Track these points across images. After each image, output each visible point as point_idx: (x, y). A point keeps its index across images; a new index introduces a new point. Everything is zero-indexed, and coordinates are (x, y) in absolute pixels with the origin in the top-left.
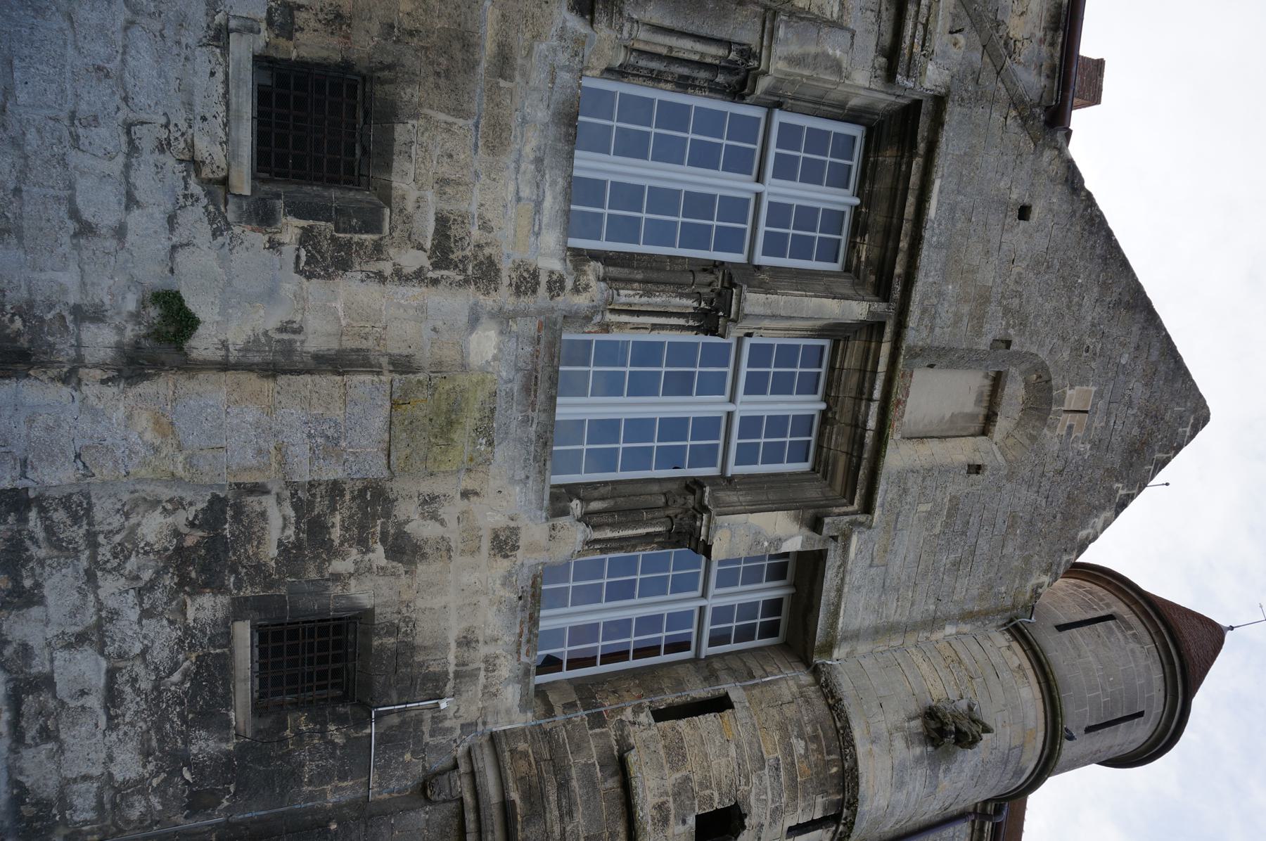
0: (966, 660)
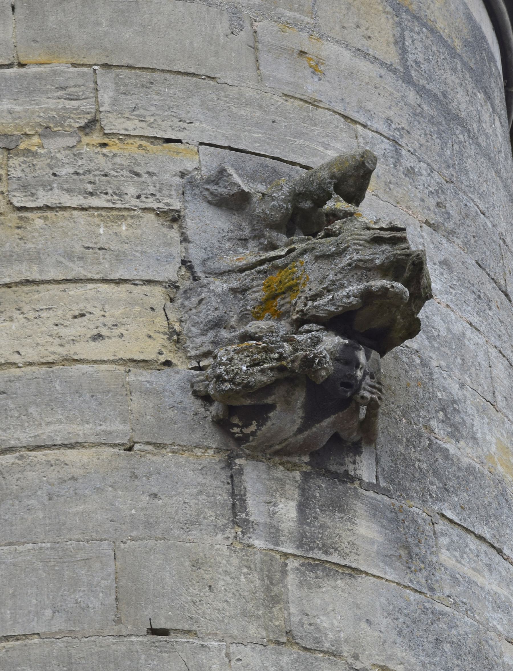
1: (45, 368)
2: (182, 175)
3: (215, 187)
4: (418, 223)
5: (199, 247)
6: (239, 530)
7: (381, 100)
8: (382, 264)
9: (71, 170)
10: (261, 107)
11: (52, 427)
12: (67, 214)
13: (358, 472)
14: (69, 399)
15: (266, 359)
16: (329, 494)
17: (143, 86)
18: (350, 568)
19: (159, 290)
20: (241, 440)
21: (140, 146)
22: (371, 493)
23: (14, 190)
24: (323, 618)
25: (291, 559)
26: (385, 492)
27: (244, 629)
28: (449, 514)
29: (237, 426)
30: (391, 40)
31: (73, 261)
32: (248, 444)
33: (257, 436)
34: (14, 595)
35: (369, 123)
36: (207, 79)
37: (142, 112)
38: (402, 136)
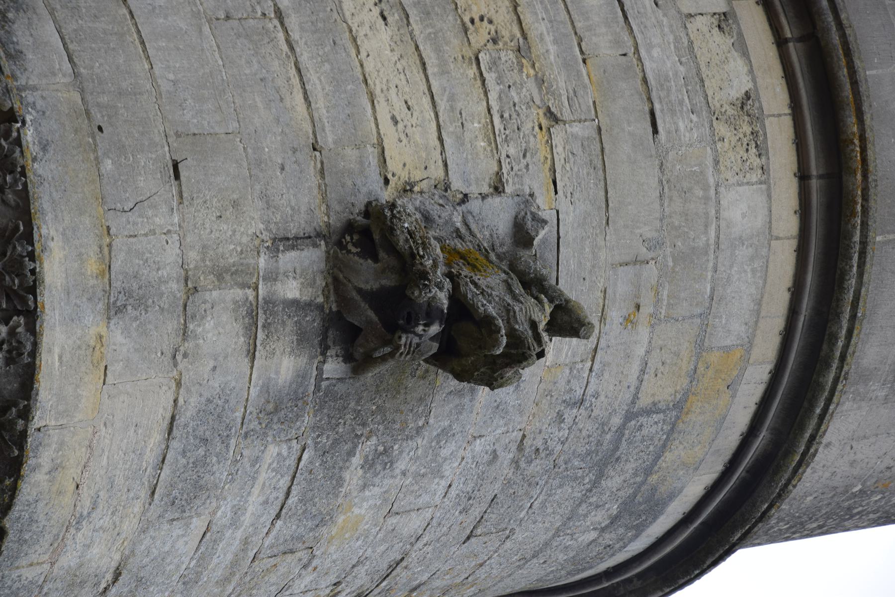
0: (548, 47)
1: (361, 77)
2: (532, 195)
4: (523, 426)
5: (481, 209)
6: (269, 244)
7: (611, 388)
8: (516, 330)
9: (516, 100)
10: (593, 267)
11: (317, 82)
12: (482, 96)
13: (330, 359)
14: (342, 96)
15: (418, 244)
17: (591, 161)
18: (255, 351)
19: (441, 173)
20: (340, 244)
21: (547, 158)
22: (315, 373)
23: (490, 54)
24: (212, 324)
25: (254, 293)
26: (317, 387)
27: (192, 247)
28: (305, 456)
29: (352, 239)
30: (656, 399)
31: (448, 101)
34: (178, 49)
37: (572, 160)
38: (586, 409)
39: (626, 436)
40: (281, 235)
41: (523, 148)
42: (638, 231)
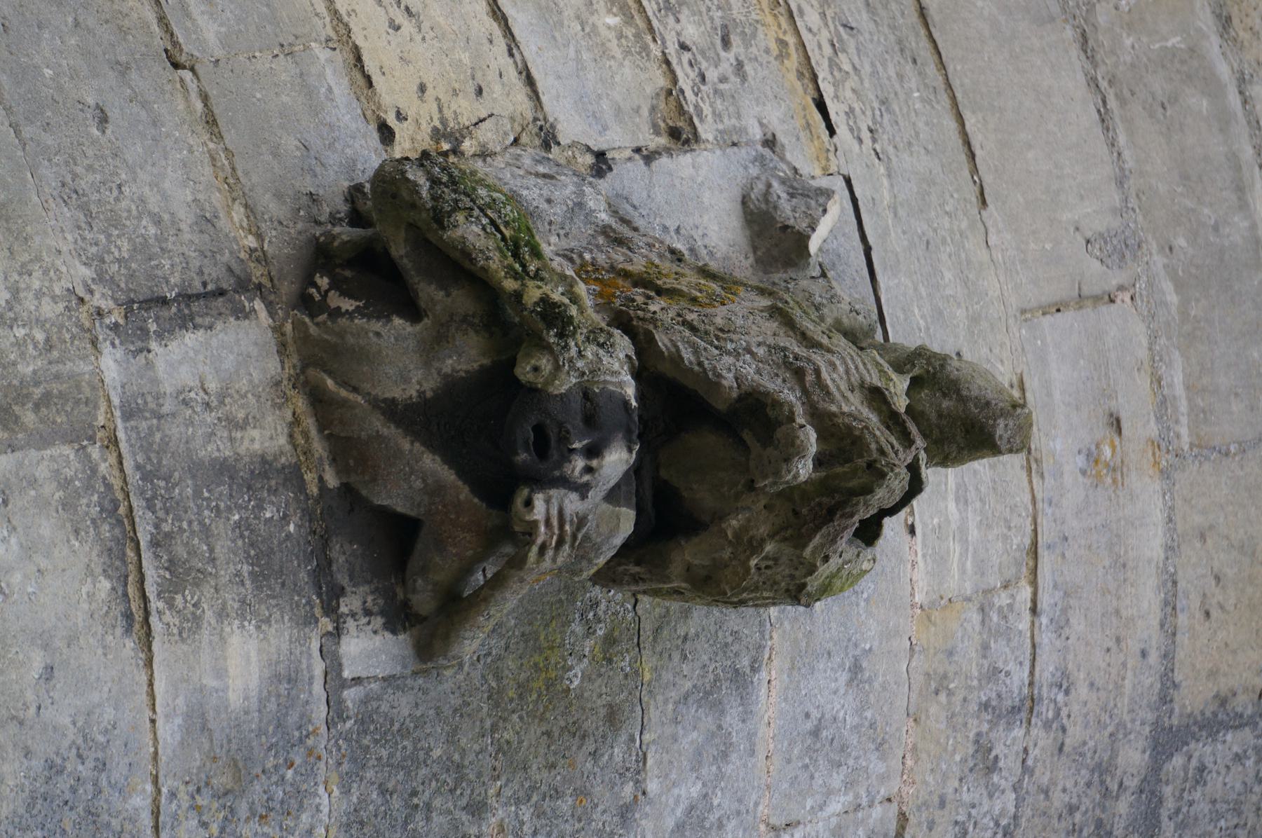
3: (784, 195)
4: (894, 786)
6: (116, 317)
10: (974, 319)
16: (280, 543)
17: (900, 42)
18: (147, 614)
19: (520, 100)
20: (305, 303)
22: (319, 667)
26: (336, 711)
30: (1224, 684)
32: (307, 320)
33: (333, 322)
35: (1044, 620)
36: (977, 189)
37: (851, 45)
38: (1047, 725)
39: (1170, 804)
40: (144, 293)
41: (718, 22)
42: (1066, 216)
